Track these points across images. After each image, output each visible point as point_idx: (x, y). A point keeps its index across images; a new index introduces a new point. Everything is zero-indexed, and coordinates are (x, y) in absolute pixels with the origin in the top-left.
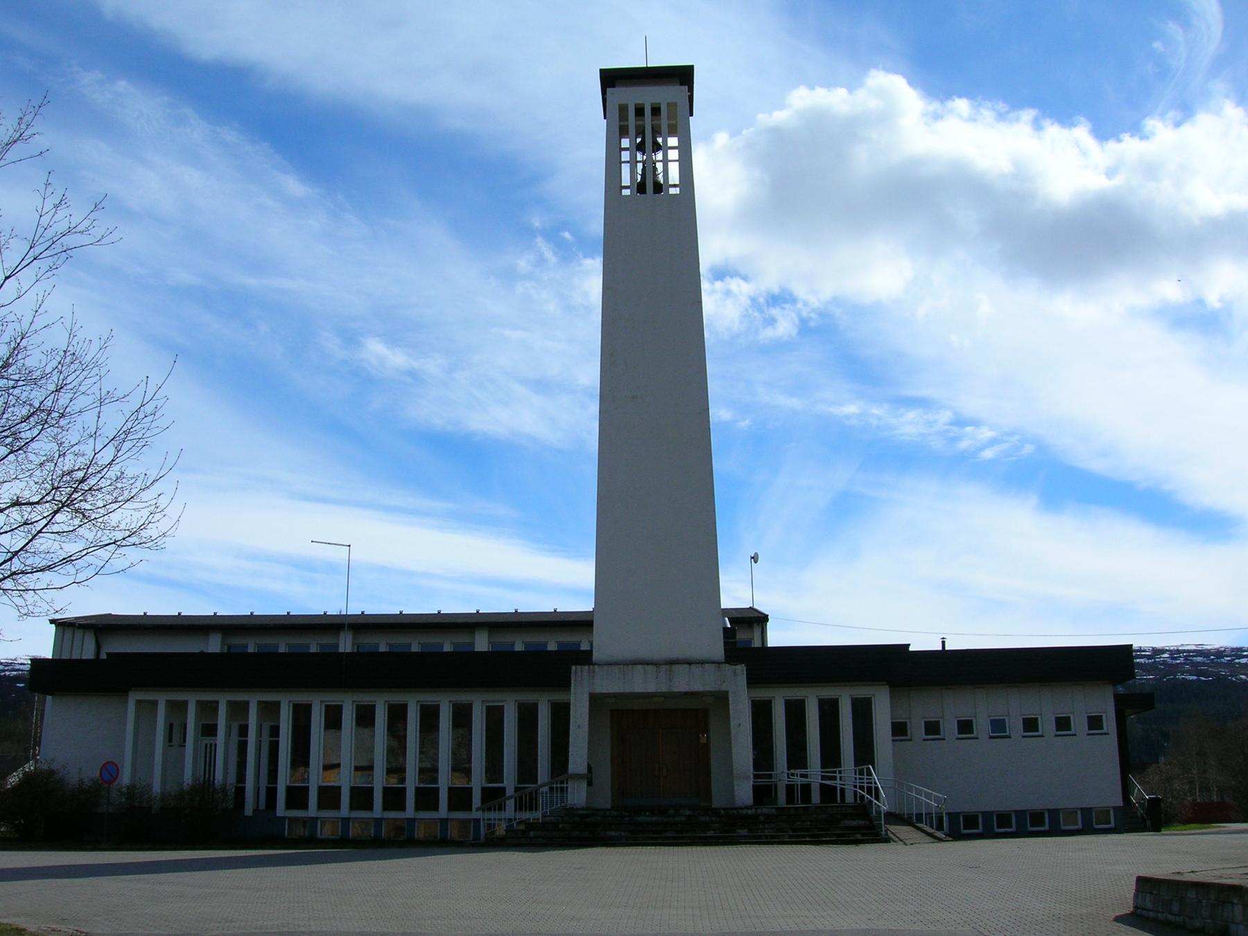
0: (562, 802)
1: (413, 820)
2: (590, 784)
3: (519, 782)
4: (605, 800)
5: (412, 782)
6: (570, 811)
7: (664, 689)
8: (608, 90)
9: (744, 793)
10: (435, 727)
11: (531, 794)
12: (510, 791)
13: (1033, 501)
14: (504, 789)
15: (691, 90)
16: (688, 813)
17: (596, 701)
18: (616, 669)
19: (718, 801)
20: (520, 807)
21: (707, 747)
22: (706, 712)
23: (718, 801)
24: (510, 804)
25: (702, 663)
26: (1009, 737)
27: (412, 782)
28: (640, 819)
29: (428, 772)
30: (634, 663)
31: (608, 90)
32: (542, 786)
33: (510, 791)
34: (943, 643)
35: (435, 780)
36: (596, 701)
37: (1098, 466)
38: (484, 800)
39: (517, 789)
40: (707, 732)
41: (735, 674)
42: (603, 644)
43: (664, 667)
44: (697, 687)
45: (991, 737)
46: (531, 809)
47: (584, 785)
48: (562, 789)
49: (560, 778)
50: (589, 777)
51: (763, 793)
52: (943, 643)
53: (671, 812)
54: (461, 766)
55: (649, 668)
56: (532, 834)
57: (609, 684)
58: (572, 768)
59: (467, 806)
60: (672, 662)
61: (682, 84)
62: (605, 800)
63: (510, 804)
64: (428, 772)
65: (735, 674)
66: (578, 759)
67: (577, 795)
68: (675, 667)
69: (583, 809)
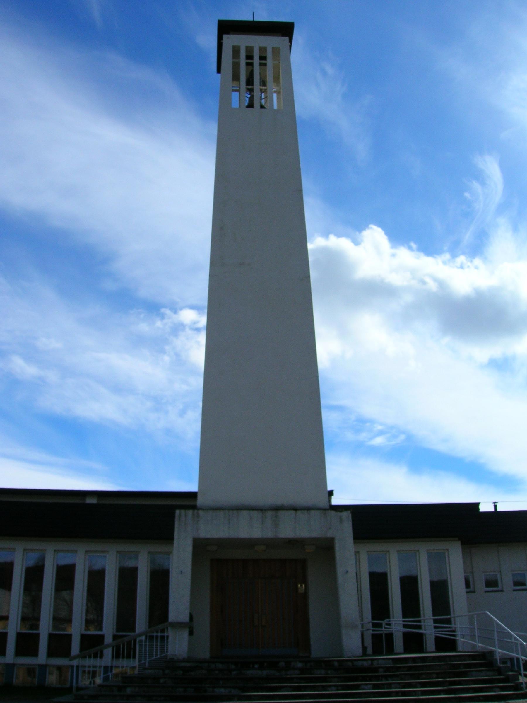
0: (162, 651)
1: (13, 665)
2: (191, 633)
3: (118, 630)
4: (204, 652)
5: (45, 627)
6: (171, 664)
7: (269, 534)
8: (225, 37)
9: (352, 643)
10: (250, 696)
11: (129, 643)
12: (108, 639)
13: (404, 469)
14: (102, 637)
15: (291, 41)
16: (300, 665)
17: (200, 546)
18: (221, 513)
19: (318, 649)
20: (117, 654)
21: (305, 596)
22: (303, 563)
23: (318, 649)
24: (108, 653)
25: (308, 509)
26: (502, 591)
27: (45, 627)
28: (250, 673)
29: (62, 619)
30: (239, 508)
31: (225, 37)
32: (140, 635)
33: (108, 639)
34: (495, 507)
35: (37, 627)
36: (200, 546)
37: (442, 448)
38: (82, 648)
39: (115, 637)
40: (304, 581)
41: (341, 520)
42: (200, 501)
43: (270, 513)
44: (303, 533)
45: (514, 590)
46: (129, 657)
47: (185, 634)
48: (163, 638)
49: (160, 627)
50: (190, 626)
51: (382, 642)
52: (495, 507)
53: (282, 664)
54: (95, 617)
55: (255, 514)
56: (129, 691)
57: (213, 529)
58: (173, 616)
59: (66, 653)
60: (277, 509)
61: (284, 35)
62: (204, 652)
63: (108, 653)
64: (62, 619)
65: (341, 520)
66: (179, 605)
67: (178, 645)
68: (281, 513)
69: (184, 660)
